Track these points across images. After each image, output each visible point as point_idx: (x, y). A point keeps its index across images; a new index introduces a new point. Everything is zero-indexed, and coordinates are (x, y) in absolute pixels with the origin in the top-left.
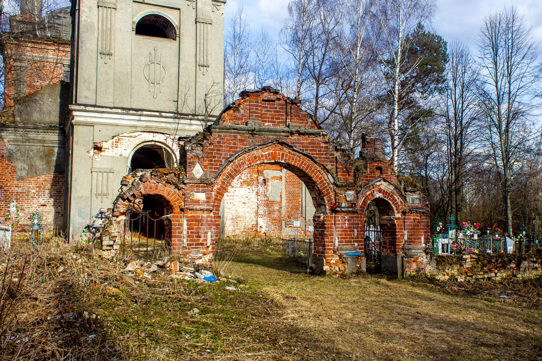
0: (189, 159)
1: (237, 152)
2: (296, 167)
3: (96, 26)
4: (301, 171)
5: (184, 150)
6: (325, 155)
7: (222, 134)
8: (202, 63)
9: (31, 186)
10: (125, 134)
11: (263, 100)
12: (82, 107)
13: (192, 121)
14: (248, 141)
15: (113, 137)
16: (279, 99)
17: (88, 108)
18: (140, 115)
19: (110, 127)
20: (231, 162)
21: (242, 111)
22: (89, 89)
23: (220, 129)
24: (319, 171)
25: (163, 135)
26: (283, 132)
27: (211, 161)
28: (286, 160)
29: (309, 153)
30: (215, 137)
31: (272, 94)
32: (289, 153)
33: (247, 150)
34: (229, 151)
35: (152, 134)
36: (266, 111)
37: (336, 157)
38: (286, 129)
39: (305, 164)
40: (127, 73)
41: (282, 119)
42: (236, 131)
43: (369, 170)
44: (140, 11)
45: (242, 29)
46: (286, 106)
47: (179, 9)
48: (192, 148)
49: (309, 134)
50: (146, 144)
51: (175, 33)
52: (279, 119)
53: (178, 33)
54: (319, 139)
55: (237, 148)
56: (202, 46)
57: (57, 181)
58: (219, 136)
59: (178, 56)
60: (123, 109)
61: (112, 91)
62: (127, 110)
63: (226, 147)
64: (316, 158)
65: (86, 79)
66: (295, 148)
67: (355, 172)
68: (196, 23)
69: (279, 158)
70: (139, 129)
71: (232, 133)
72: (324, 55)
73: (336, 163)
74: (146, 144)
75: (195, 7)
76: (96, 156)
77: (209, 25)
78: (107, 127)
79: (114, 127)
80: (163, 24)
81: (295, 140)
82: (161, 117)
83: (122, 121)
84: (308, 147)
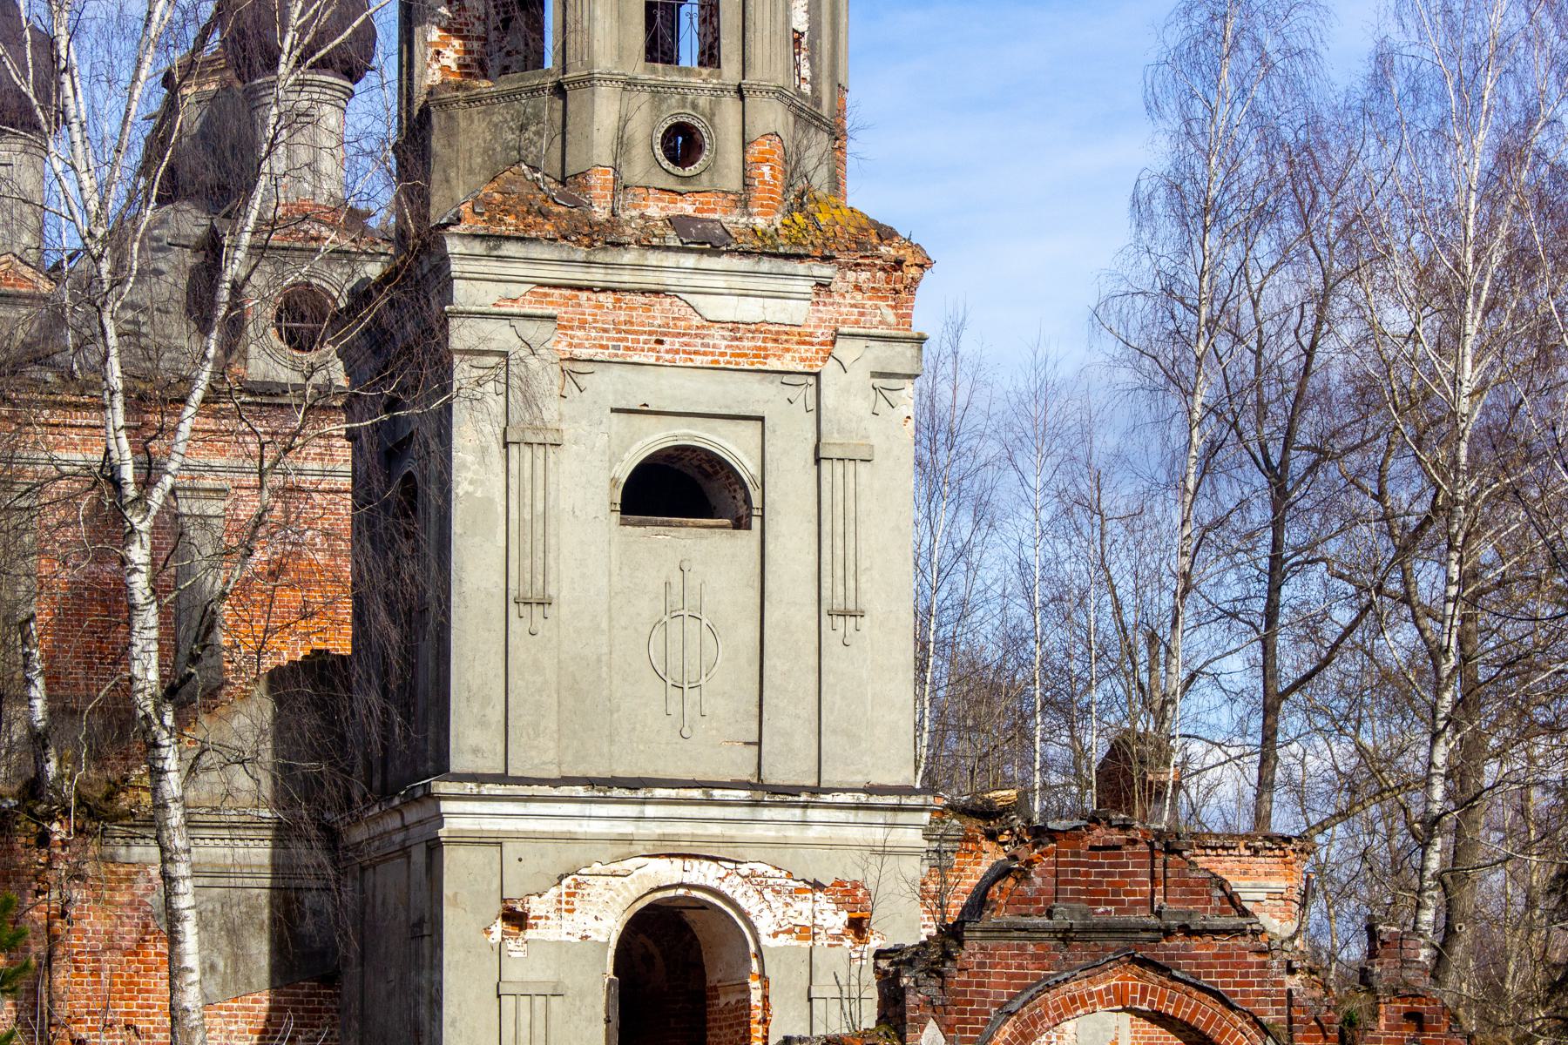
0: (912, 1010)
1: (1027, 988)
2: (1181, 1020)
3: (501, 509)
4: (1194, 1029)
5: (897, 985)
6: (1260, 984)
7: (989, 944)
8: (839, 604)
9: (233, 1027)
10: (597, 867)
11: (1092, 848)
12: (470, 787)
13: (809, 811)
14: (1054, 958)
15: (561, 878)
16: (1134, 842)
17: (488, 789)
18: (644, 802)
19: (550, 847)
20: (1010, 1014)
21: (1038, 881)
22: (483, 723)
23: (984, 930)
24: (1241, 1030)
25: (714, 865)
26: (1146, 930)
27: (964, 1012)
28: (1151, 1003)
29: (1215, 984)
30: (971, 951)
31: (1115, 830)
32: (1161, 984)
33: (1051, 981)
34: (1007, 986)
35: (678, 862)
36: (1098, 874)
37: (1290, 991)
38: (1153, 921)
39: (1204, 1013)
40: (599, 660)
41: (1142, 893)
42: (1023, 934)
43: (1383, 1021)
44: (633, 442)
45: (962, 399)
46: (1153, 858)
47: (762, 419)
48: (916, 982)
49: (1215, 932)
50: (659, 895)
51: (747, 500)
52: (1133, 893)
53: (756, 502)
54: (1242, 942)
55: (1025, 976)
56: (839, 542)
57: (314, 1011)
58: (982, 948)
59: (757, 585)
60: (590, 782)
61: (554, 727)
62: (603, 786)
63: (1000, 975)
64: (1235, 994)
65: (474, 688)
66: (1176, 973)
67: (1341, 1031)
68: (818, 461)
69: (1134, 1000)
70: (639, 848)
71: (1014, 938)
72: (1310, 354)
73: (1290, 1005)
74: (659, 895)
75: (812, 405)
76: (511, 944)
77: (861, 466)
78: (541, 845)
79: (561, 845)
80: (699, 467)
81: (1177, 947)
82: (711, 802)
83: (585, 822)
84: (1211, 966)
